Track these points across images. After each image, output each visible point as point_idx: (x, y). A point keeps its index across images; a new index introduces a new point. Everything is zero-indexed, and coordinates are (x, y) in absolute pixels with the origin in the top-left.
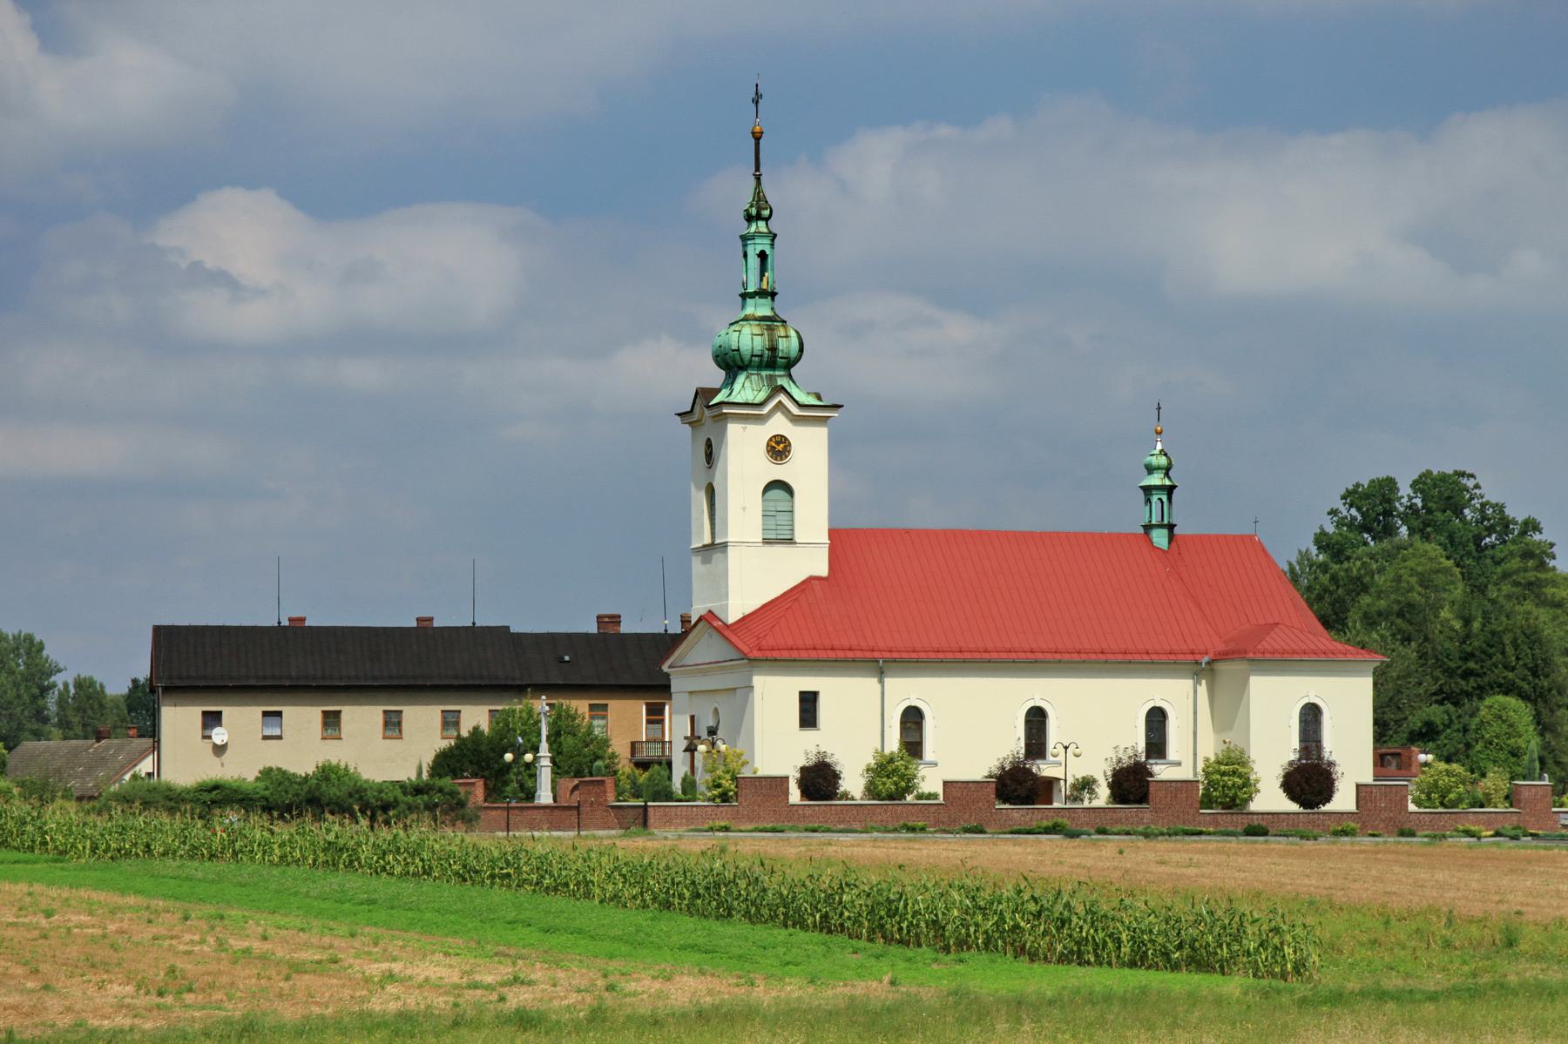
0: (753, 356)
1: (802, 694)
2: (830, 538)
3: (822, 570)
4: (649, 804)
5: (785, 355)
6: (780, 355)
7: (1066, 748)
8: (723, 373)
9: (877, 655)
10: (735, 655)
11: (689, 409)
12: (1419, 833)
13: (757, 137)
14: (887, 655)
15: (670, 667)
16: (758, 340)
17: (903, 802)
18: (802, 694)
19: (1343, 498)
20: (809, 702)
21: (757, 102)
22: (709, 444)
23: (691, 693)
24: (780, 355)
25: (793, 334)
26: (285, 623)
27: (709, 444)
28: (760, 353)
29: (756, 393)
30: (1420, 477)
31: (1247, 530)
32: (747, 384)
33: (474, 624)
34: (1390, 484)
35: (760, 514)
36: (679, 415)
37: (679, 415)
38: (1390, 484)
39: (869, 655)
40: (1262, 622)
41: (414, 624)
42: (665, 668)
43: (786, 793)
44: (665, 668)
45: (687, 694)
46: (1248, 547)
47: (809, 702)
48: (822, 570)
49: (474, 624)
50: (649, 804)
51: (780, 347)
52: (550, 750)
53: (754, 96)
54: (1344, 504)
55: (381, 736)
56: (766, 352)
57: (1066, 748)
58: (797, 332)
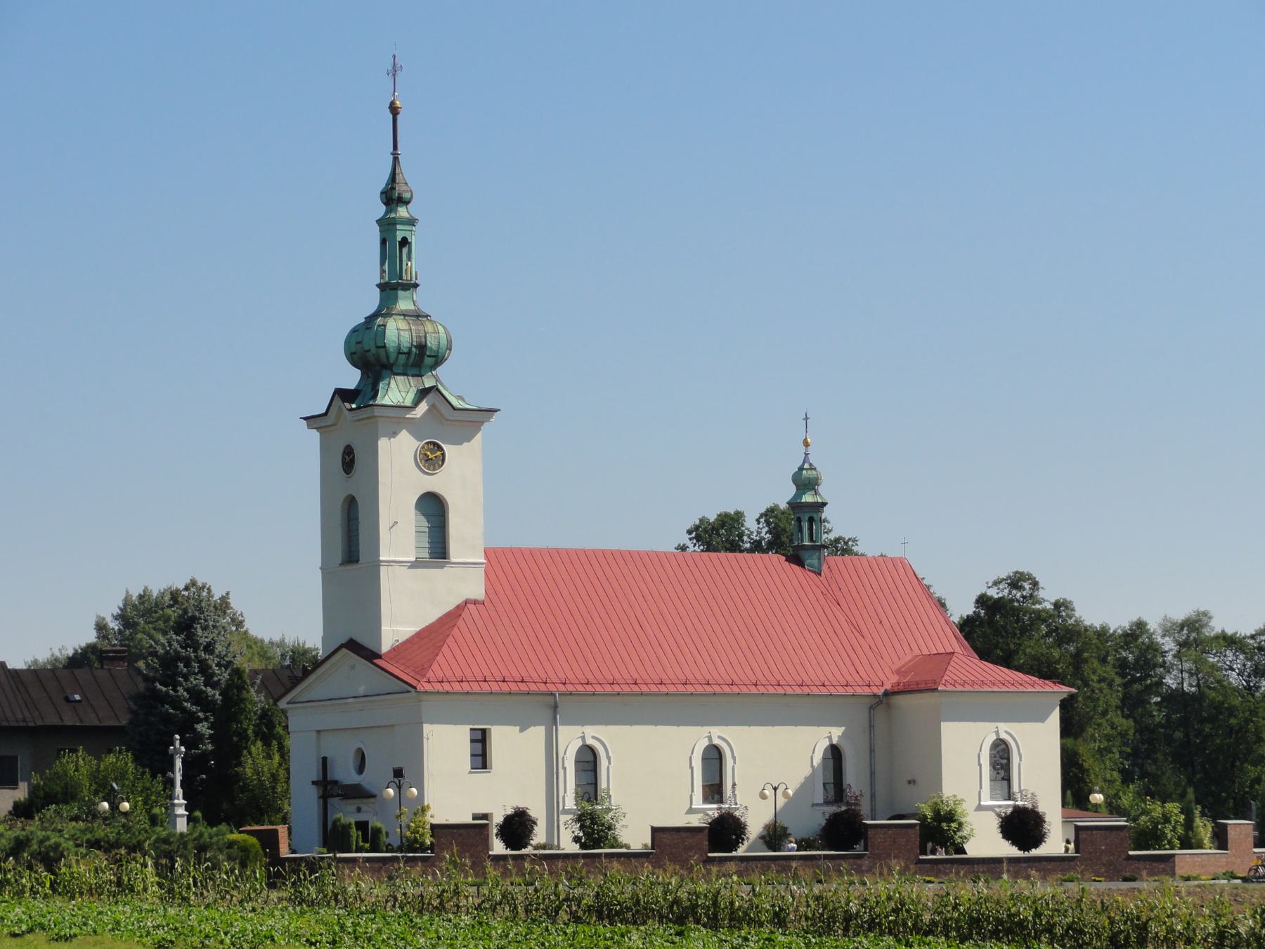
0: (399, 353)
7: (775, 789)
9: (552, 688)
10: (640, 685)
11: (324, 411)
13: (394, 110)
14: (562, 688)
15: (288, 703)
17: (734, 854)
19: (689, 532)
22: (349, 453)
23: (319, 732)
24: (428, 353)
25: (441, 329)
27: (349, 453)
30: (768, 510)
34: (737, 518)
35: (413, 530)
36: (305, 419)
37: (305, 419)
38: (737, 518)
39: (543, 688)
40: (926, 652)
43: (487, 845)
47: (481, 741)
53: (390, 68)
54: (690, 539)
56: (414, 349)
57: (775, 789)
58: (444, 328)
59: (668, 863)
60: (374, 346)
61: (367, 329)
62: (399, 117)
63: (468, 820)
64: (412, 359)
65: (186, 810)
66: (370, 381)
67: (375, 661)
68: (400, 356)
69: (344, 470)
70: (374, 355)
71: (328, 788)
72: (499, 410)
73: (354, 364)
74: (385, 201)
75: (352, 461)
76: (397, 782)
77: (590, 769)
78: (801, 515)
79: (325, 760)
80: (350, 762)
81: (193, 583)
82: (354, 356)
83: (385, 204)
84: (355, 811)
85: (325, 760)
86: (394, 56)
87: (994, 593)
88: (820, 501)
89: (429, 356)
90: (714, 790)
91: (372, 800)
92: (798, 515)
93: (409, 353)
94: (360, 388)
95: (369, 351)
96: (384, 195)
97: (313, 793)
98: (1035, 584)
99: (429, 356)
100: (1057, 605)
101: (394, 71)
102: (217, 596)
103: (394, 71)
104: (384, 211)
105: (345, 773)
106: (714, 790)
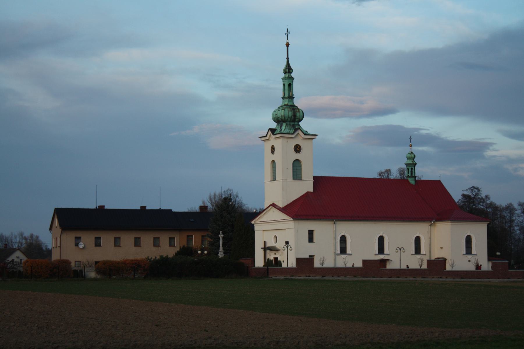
0: (288, 118)
1: (309, 231)
2: (313, 179)
3: (311, 190)
4: (266, 267)
5: (298, 118)
6: (297, 118)
7: (400, 249)
8: (276, 124)
11: (265, 135)
12: (326, 276)
13: (288, 45)
15: (254, 222)
16: (290, 113)
18: (309, 231)
20: (311, 233)
21: (287, 35)
23: (263, 230)
24: (297, 118)
26: (98, 208)
28: (290, 117)
29: (289, 130)
31: (438, 179)
32: (287, 127)
33: (160, 208)
41: (139, 208)
42: (253, 222)
44: (253, 222)
45: (262, 231)
46: (308, 193)
47: (311, 233)
48: (311, 190)
49: (160, 208)
50: (269, 267)
51: (297, 115)
52: (223, 249)
55: (113, 245)
57: (400, 249)
59: (493, 205)
60: (281, 116)
61: (279, 111)
62: (289, 47)
63: (308, 257)
64: (292, 119)
65: (224, 253)
66: (280, 126)
67: (276, 207)
68: (288, 119)
69: (272, 153)
70: (280, 118)
71: (266, 249)
72: (318, 135)
73: (275, 121)
74: (284, 72)
75: (271, 149)
76: (287, 246)
77: (300, 136)
78: (409, 167)
79: (265, 242)
80: (273, 240)
81: (229, 189)
82: (275, 119)
83: (284, 73)
84: (274, 254)
85: (265, 242)
86: (287, 29)
87: (466, 193)
88: (414, 163)
89: (297, 119)
90: (381, 250)
91: (279, 251)
92: (408, 167)
93: (291, 118)
94: (276, 128)
95: (279, 117)
96: (284, 71)
97: (262, 252)
98: (479, 190)
99: (297, 119)
100: (486, 196)
101: (288, 33)
102: (235, 194)
103: (288, 33)
104: (304, 130)
105: (271, 243)
106: (381, 250)
